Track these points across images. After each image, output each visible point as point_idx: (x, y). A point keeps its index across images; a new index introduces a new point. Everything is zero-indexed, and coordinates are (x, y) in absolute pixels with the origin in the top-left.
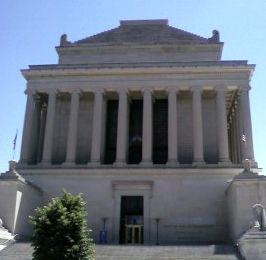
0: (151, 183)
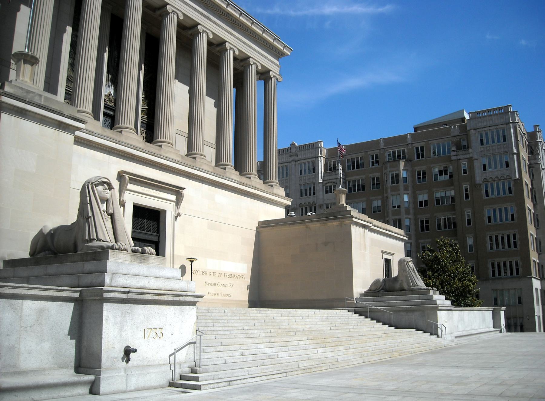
0: (178, 191)
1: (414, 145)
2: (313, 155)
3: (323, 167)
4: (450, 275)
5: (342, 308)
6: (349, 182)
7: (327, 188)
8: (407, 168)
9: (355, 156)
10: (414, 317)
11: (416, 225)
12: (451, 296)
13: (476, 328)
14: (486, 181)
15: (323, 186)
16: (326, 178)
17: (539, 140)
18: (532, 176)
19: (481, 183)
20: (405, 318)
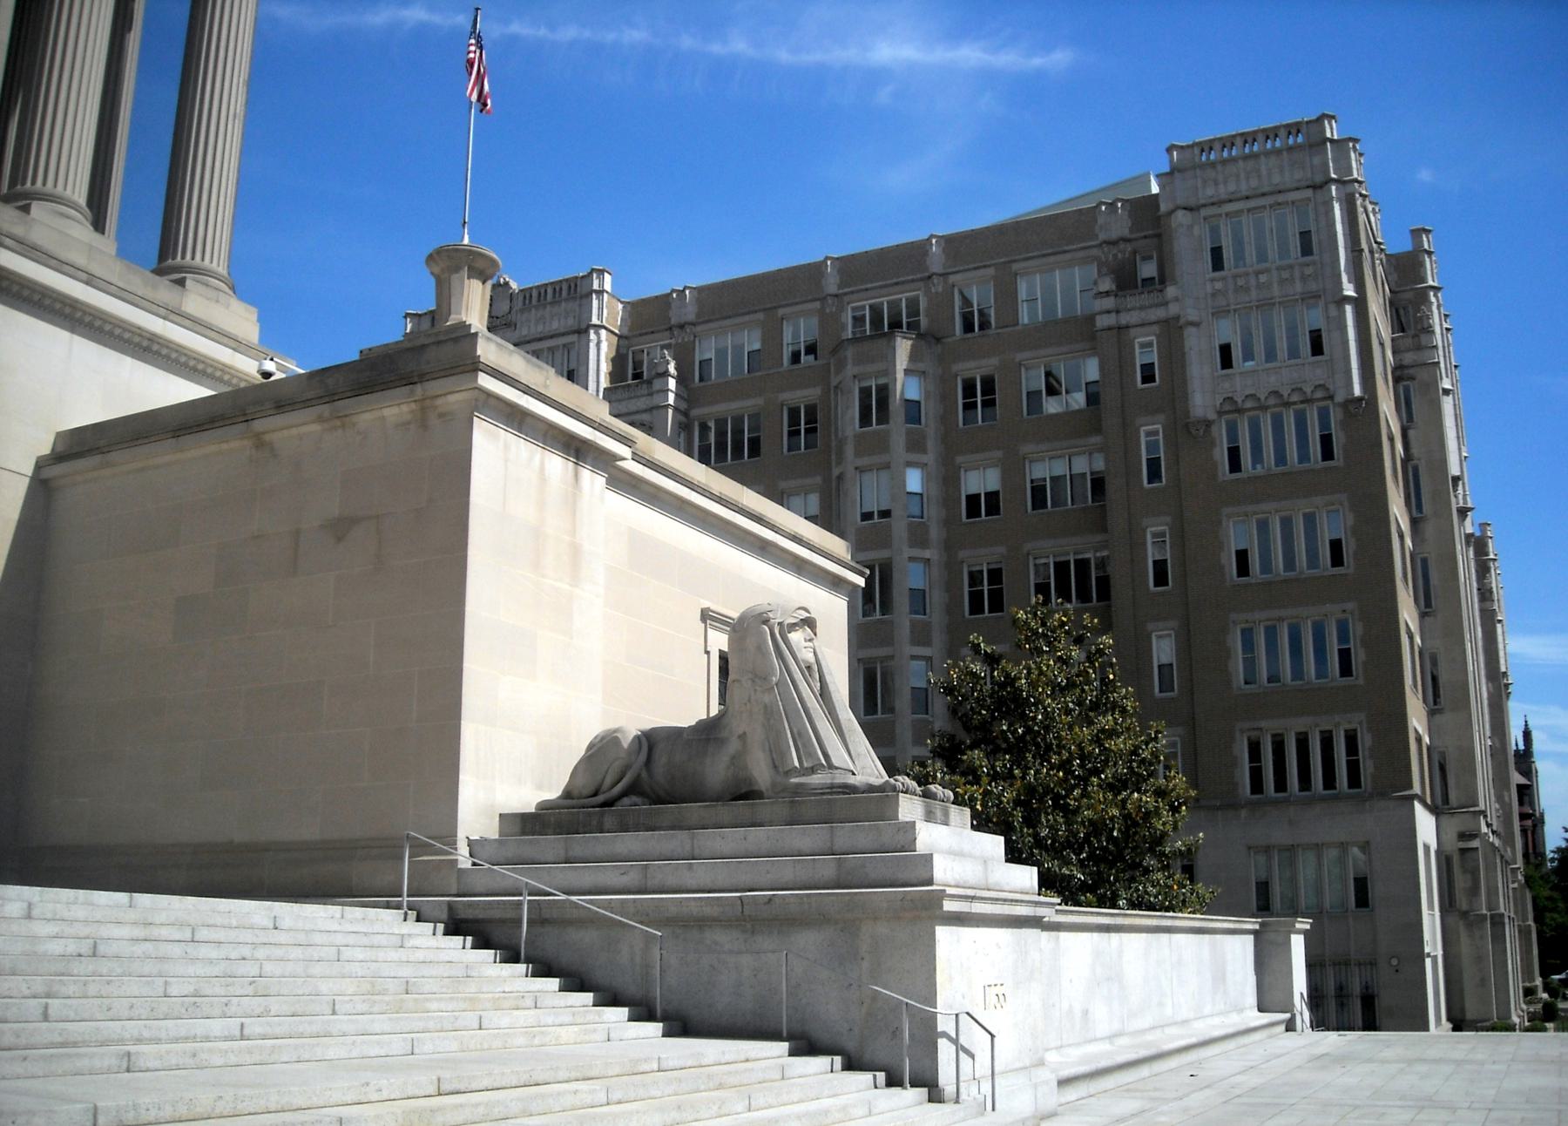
1: (952, 279)
2: (571, 322)
4: (1065, 765)
5: (378, 893)
6: (704, 428)
8: (921, 366)
10: (787, 966)
11: (951, 586)
12: (1067, 863)
13: (1185, 1013)
14: (1231, 407)
17: (1431, 283)
18: (1405, 406)
19: (1212, 416)
20: (740, 966)
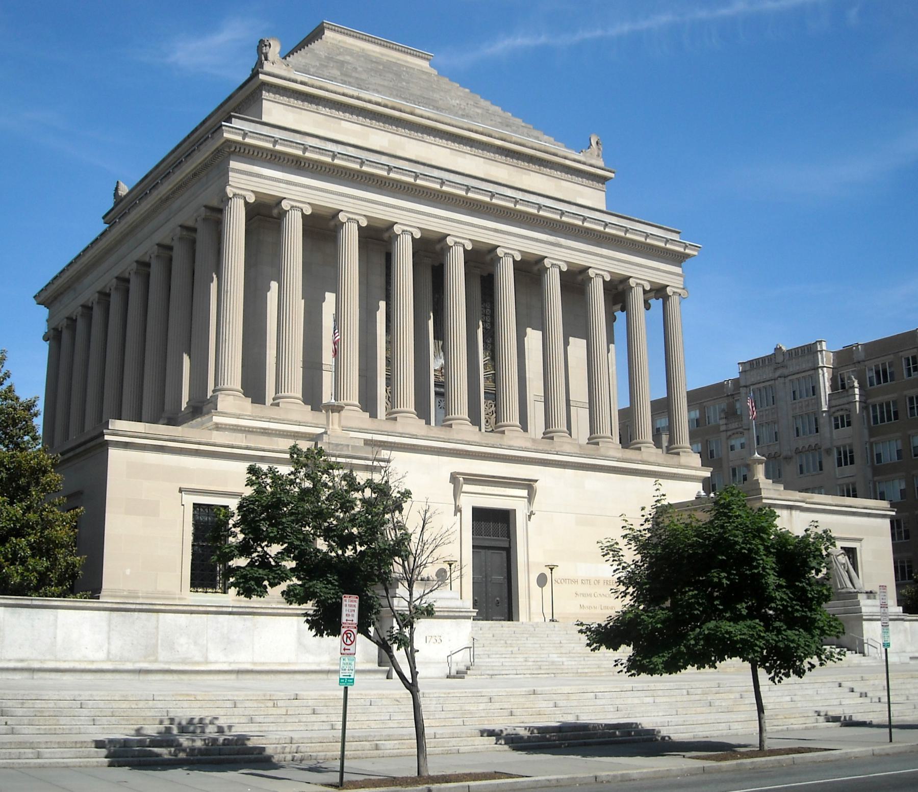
0: (528, 485)
3: (827, 384)
7: (836, 419)
9: (879, 361)
15: (830, 416)
16: (834, 403)
